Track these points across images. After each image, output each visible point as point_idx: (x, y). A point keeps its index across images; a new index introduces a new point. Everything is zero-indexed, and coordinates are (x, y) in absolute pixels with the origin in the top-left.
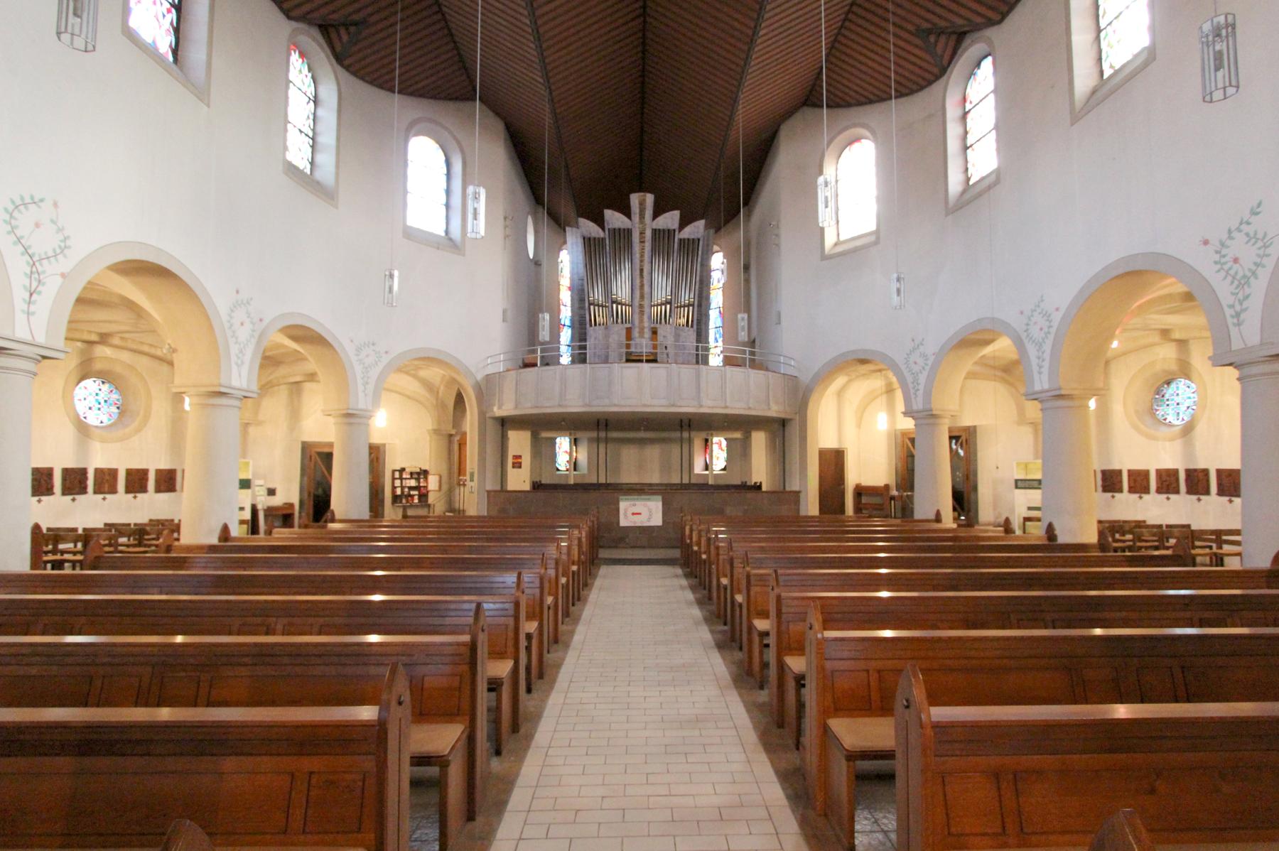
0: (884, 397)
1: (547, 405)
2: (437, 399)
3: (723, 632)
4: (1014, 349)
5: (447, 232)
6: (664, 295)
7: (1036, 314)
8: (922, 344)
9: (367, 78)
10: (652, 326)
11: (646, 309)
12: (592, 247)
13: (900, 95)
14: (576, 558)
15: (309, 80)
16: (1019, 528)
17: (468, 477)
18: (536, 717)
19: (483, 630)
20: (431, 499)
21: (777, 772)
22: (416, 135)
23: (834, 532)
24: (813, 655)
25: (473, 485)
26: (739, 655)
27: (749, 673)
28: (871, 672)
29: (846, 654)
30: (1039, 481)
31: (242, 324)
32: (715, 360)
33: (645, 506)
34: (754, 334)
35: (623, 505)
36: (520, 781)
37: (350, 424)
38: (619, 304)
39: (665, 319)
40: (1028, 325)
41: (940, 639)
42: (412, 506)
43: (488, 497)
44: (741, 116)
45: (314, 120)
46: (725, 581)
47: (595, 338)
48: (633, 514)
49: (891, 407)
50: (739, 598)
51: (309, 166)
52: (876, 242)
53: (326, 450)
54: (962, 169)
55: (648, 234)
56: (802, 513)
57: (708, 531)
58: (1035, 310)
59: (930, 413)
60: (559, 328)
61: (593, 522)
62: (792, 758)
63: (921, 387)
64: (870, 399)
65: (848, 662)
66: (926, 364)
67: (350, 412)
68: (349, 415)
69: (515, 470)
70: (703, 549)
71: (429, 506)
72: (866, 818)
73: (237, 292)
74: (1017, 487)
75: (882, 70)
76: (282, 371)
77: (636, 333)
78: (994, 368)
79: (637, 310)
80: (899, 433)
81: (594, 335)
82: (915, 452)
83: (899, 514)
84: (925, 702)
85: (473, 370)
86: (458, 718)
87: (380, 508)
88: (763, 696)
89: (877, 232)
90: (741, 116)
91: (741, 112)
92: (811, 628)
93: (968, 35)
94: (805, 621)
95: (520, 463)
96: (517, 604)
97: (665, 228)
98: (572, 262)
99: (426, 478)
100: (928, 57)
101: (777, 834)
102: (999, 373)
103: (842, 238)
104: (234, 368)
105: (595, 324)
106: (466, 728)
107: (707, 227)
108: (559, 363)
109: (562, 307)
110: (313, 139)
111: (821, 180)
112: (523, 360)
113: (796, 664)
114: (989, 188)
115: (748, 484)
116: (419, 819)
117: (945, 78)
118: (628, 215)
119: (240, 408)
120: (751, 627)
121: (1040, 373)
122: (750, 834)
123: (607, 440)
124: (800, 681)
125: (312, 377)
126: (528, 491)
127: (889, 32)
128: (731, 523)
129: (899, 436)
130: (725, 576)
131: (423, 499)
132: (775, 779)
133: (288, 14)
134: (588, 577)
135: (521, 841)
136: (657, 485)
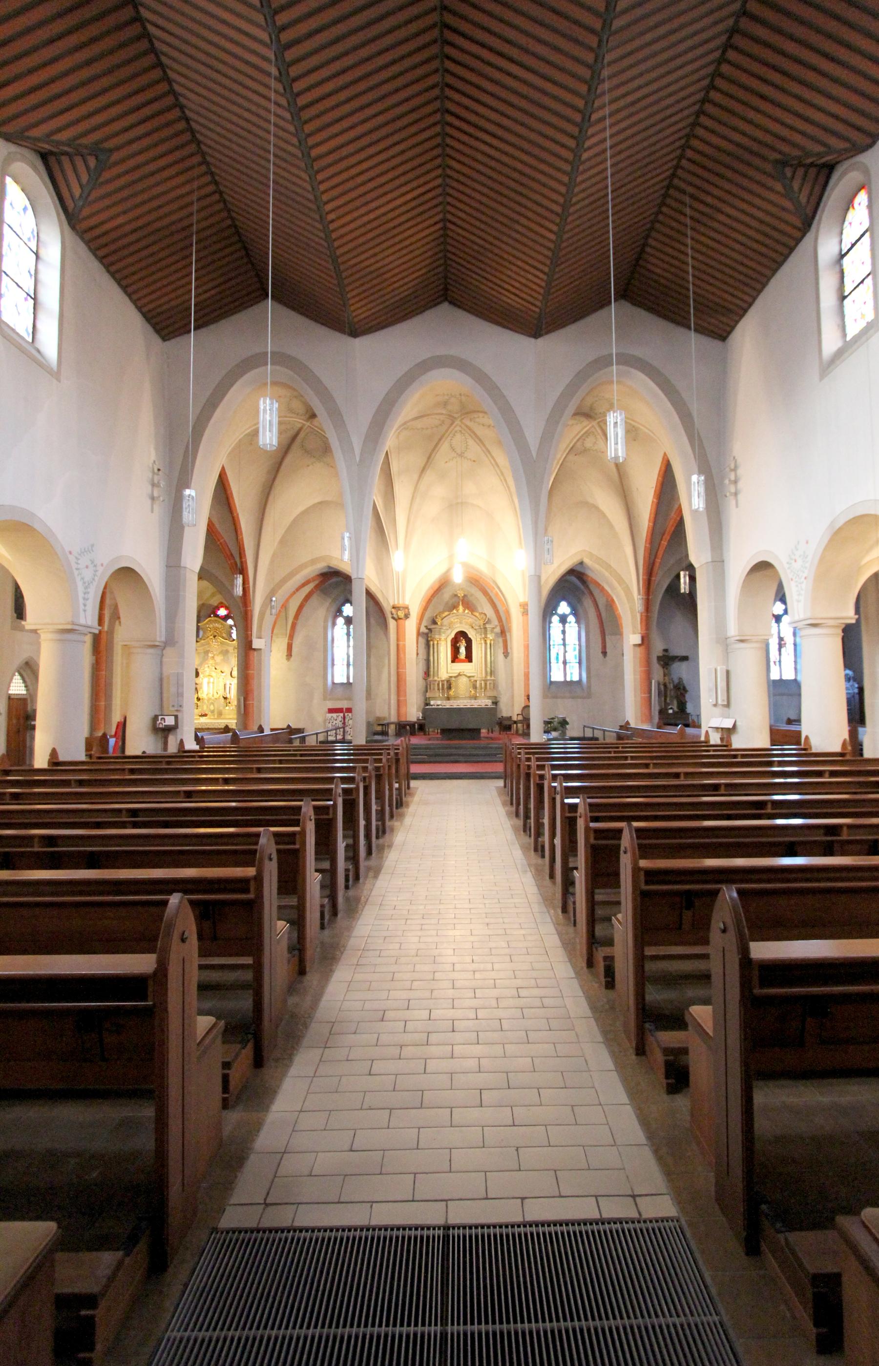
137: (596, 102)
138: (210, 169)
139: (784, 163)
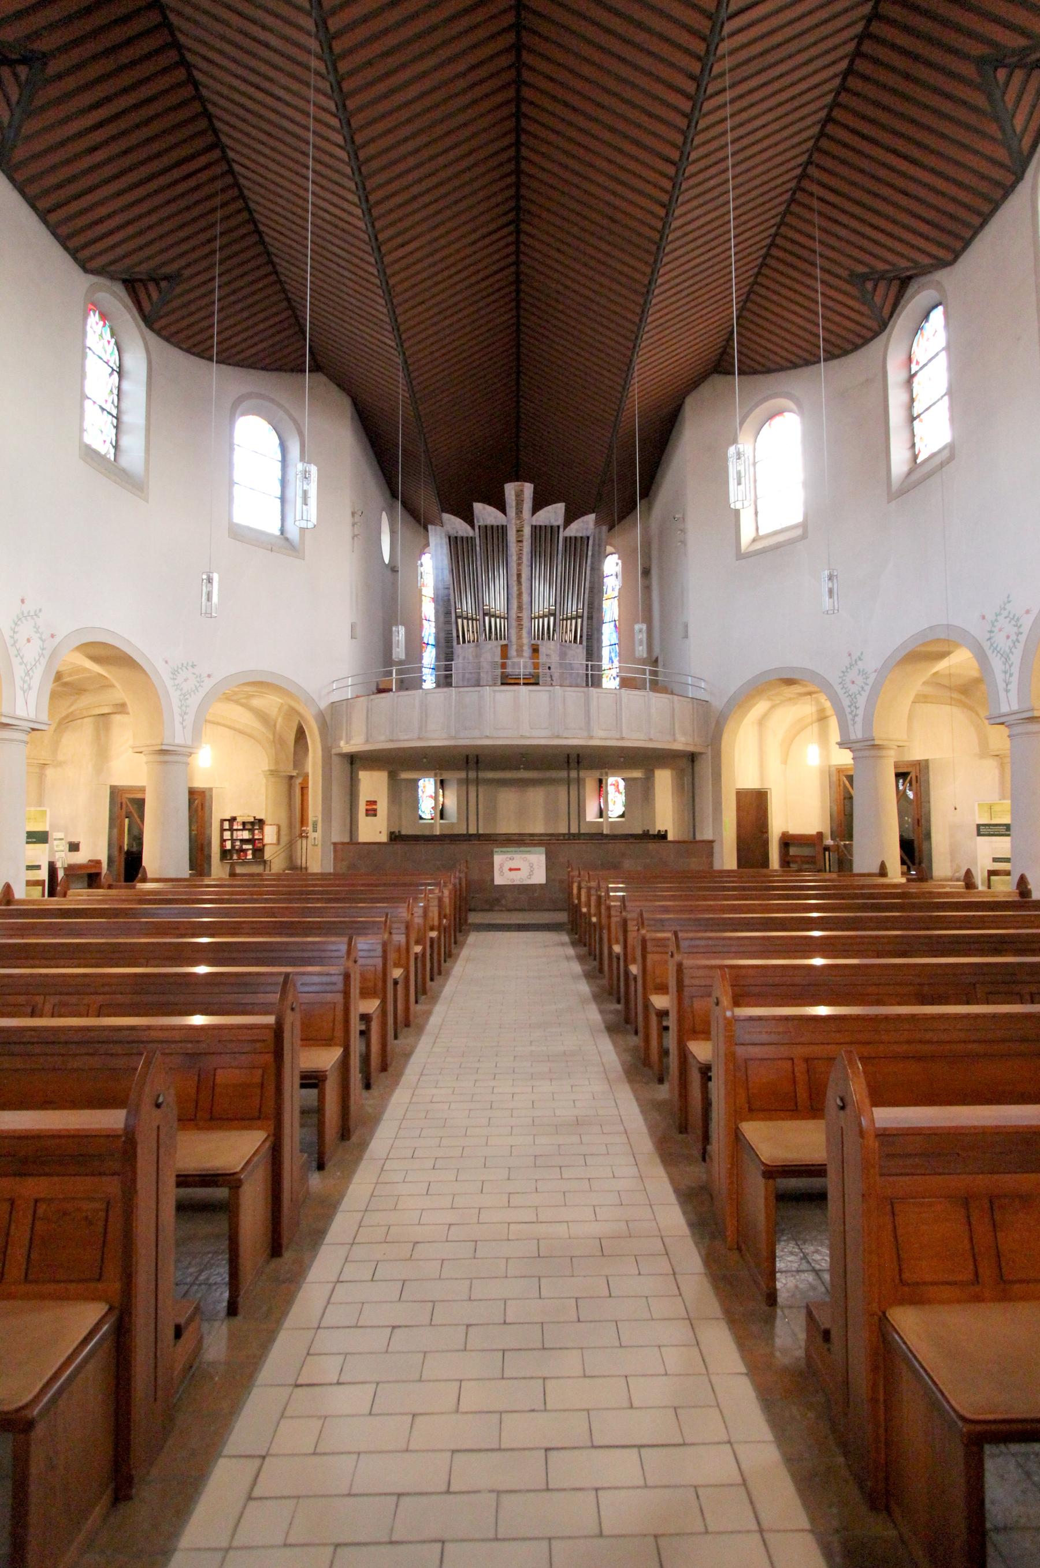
0: (816, 727)
1: (406, 737)
2: (274, 734)
3: (617, 1011)
4: (975, 664)
5: (282, 531)
6: (546, 605)
7: (1001, 618)
8: (860, 659)
9: (184, 346)
10: (533, 642)
11: (525, 622)
12: (458, 547)
13: (831, 356)
14: (436, 923)
15: (112, 347)
16: (983, 884)
17: (310, 828)
18: (373, 1121)
19: (293, 1009)
20: (267, 856)
21: (677, 1191)
22: (243, 414)
23: (755, 889)
24: (722, 1039)
25: (315, 836)
26: (635, 1041)
27: (646, 1062)
28: (795, 1061)
29: (764, 1038)
30: (1008, 827)
31: (29, 641)
32: (610, 682)
33: (525, 860)
34: (657, 651)
35: (498, 859)
36: (346, 1204)
37: (166, 762)
38: (493, 616)
39: (547, 635)
40: (991, 632)
41: (886, 1018)
42: (245, 863)
43: (335, 851)
44: (636, 386)
45: (118, 395)
46: (617, 949)
47: (464, 658)
48: (511, 870)
49: (823, 738)
50: (634, 969)
51: (112, 451)
52: (804, 537)
53: (139, 796)
54: (909, 445)
55: (527, 531)
56: (717, 866)
57: (599, 888)
58: (1000, 614)
59: (872, 743)
60: (421, 648)
61: (460, 879)
62: (695, 1172)
63: (861, 712)
64: (798, 729)
65: (766, 1048)
66: (867, 684)
67: (164, 747)
68: (163, 752)
69: (369, 818)
70: (593, 911)
71: (265, 862)
72: (792, 1253)
73: (23, 601)
74: (979, 834)
75: (809, 326)
76: (83, 702)
77: (513, 652)
78: (950, 688)
79: (514, 623)
80: (833, 769)
81: (463, 653)
82: (853, 792)
83: (835, 868)
84: (867, 1101)
85: (315, 697)
86: (259, 1123)
87: (206, 866)
88: (664, 1092)
89: (804, 525)
90: (636, 386)
91: (636, 380)
92: (717, 1004)
93: (913, 281)
94: (710, 995)
95: (375, 810)
96: (347, 977)
97: (547, 524)
98: (436, 568)
99: (261, 829)
100: (864, 309)
101: (674, 1274)
102: (955, 695)
103: (761, 533)
104: (19, 693)
105: (464, 642)
106: (269, 1136)
107: (598, 522)
108: (421, 688)
109: (424, 622)
110: (117, 418)
111: (732, 450)
112: (378, 685)
113: (701, 1050)
114: (942, 465)
115: (651, 833)
116: (210, 1255)
117: (883, 337)
118: (503, 509)
119: (27, 743)
120: (647, 1005)
121: (1007, 691)
122: (639, 1274)
123: (478, 782)
124: (706, 1071)
125: (121, 708)
126: (384, 843)
127: (816, 278)
128: (629, 879)
129: (834, 773)
130: (617, 942)
131: (258, 854)
132: (672, 1198)
133: (85, 267)
134: (453, 945)
135: (338, 1285)
136: (541, 835)
137: (700, 122)
138: (206, 110)
139: (998, 63)
